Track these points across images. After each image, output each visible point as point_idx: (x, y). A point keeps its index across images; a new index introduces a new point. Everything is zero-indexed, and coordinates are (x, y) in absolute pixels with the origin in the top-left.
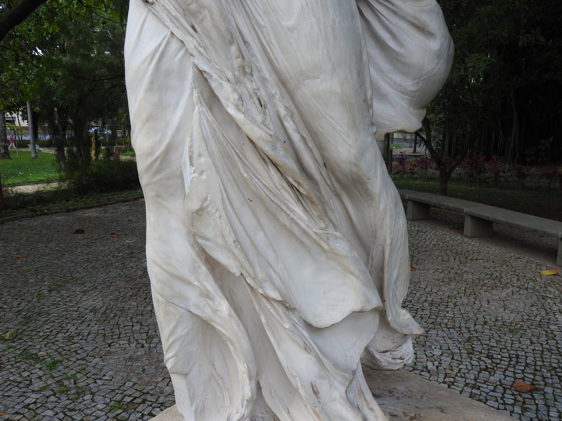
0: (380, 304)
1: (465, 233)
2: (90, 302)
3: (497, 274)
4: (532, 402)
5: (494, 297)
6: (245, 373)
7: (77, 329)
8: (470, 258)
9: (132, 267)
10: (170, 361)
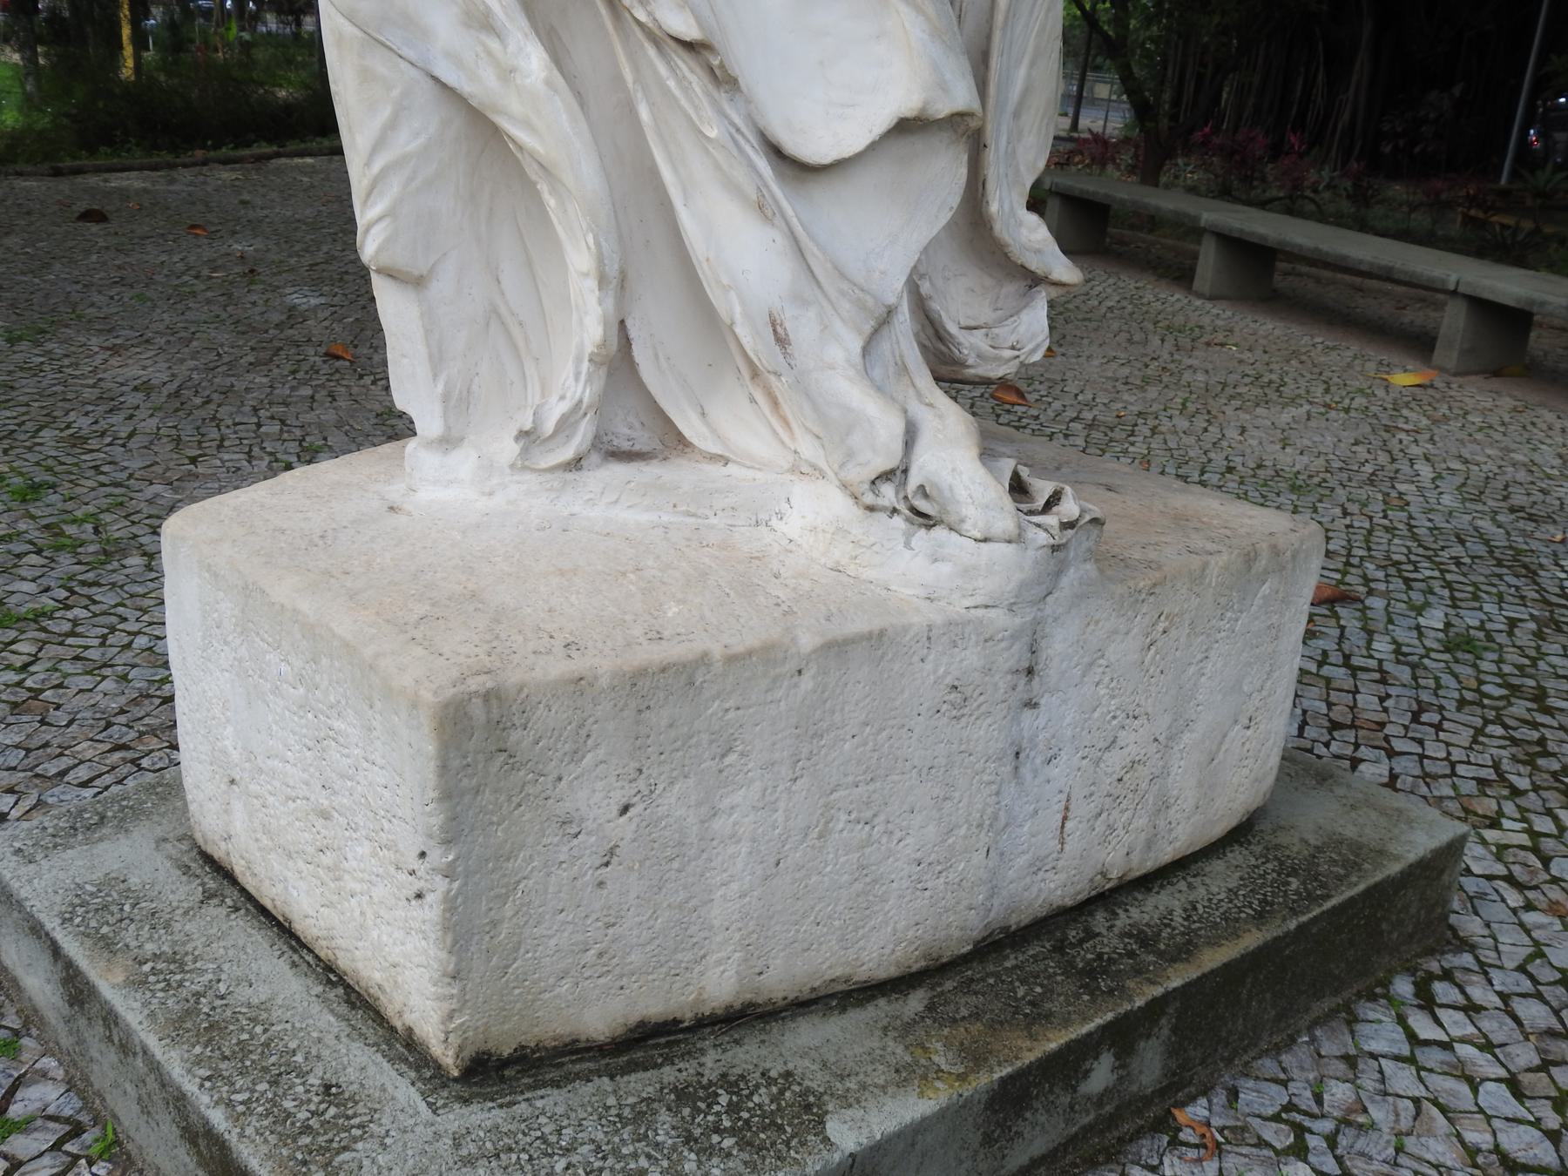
0: (976, 106)
1: (1197, 284)
2: (133, 369)
3: (1274, 377)
4: (1333, 622)
5: (1258, 422)
6: (586, 275)
7: (96, 422)
8: (1203, 340)
9: (254, 304)
10: (373, 231)
